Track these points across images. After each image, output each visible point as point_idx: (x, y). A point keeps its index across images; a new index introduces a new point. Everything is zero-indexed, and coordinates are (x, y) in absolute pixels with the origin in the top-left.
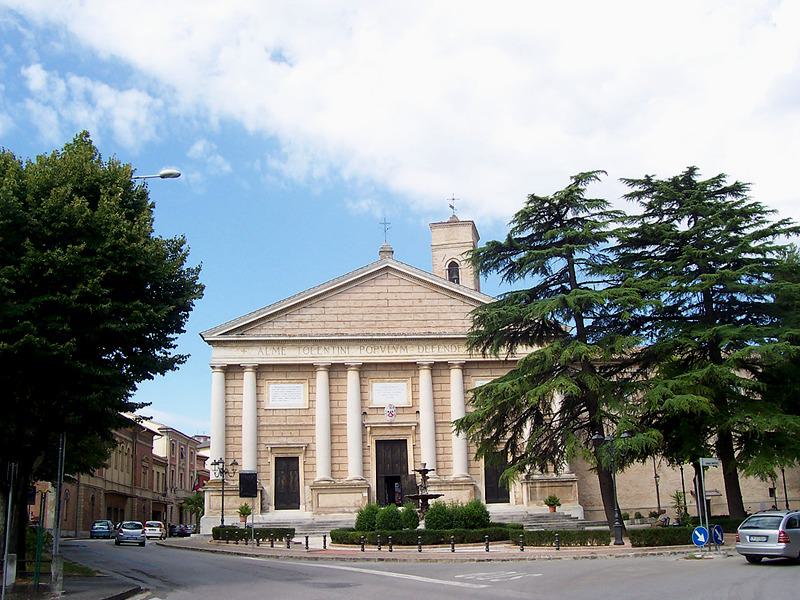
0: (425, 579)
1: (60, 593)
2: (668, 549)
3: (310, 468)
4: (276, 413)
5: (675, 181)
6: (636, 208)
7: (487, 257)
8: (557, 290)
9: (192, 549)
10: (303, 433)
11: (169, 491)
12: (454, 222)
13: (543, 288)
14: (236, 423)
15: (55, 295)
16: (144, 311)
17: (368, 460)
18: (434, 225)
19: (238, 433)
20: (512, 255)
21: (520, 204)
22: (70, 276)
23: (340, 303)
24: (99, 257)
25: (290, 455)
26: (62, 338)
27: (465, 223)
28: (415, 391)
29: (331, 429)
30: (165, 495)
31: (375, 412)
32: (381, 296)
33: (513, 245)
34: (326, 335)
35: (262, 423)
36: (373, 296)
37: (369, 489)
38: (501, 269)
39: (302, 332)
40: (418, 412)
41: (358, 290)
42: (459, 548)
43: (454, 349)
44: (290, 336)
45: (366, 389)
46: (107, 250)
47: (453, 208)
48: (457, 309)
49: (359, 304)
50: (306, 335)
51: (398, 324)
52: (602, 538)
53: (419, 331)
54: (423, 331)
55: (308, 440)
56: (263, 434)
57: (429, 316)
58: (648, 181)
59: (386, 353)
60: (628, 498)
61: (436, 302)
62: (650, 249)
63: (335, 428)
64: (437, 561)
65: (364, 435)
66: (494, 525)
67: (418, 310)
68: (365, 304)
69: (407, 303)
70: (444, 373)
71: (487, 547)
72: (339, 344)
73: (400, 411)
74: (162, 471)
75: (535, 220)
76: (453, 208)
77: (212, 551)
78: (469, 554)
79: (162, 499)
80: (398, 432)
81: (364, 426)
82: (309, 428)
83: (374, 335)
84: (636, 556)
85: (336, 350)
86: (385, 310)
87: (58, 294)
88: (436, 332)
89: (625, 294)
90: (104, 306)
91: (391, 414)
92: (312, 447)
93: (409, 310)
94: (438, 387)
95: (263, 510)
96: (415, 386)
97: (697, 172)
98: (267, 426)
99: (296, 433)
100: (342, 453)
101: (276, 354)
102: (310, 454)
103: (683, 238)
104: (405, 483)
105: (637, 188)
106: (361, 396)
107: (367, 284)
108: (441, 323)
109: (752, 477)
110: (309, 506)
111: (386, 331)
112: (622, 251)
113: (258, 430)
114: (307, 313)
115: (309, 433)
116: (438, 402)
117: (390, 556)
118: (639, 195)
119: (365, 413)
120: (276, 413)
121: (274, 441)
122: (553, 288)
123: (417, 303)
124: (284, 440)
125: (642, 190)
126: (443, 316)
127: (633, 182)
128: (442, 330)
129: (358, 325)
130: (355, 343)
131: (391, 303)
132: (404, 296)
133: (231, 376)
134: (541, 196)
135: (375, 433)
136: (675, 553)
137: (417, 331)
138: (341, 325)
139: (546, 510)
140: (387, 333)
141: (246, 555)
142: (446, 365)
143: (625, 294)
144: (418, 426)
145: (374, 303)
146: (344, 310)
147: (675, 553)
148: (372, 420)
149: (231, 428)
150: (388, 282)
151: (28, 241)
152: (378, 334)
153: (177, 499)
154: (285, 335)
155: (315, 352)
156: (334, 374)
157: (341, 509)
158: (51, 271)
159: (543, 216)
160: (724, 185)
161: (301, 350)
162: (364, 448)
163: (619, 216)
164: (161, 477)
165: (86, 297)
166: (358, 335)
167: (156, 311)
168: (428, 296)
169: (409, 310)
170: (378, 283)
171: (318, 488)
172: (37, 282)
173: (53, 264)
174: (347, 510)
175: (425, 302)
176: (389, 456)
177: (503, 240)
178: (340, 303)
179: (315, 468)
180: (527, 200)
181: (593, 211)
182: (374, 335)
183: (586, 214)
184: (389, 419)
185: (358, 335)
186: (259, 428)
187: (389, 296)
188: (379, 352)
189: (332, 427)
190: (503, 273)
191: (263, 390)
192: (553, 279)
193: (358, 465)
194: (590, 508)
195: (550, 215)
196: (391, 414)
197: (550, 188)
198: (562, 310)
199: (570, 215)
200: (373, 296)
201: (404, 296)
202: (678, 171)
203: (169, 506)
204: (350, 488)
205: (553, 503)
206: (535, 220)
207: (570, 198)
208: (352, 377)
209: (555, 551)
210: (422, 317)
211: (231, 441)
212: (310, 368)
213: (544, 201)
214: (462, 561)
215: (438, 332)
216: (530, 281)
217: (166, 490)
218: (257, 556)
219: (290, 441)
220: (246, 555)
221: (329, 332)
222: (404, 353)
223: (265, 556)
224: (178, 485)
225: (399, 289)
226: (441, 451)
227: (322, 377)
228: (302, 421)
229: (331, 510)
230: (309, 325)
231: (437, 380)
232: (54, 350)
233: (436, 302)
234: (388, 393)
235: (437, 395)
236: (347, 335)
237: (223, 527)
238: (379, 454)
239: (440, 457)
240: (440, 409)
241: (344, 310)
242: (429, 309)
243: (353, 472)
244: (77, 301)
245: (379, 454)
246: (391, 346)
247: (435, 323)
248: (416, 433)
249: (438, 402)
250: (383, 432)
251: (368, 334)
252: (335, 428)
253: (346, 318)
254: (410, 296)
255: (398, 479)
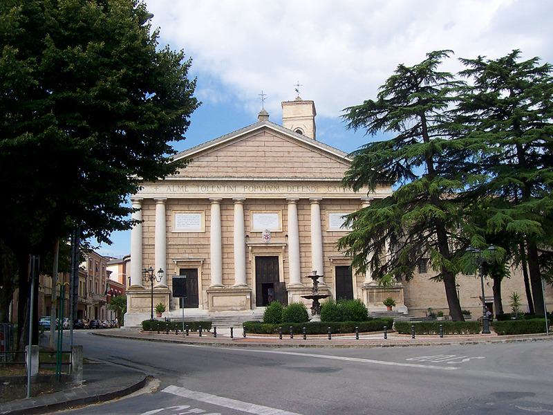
0: (374, 361)
1: (81, 382)
2: (531, 337)
3: (207, 277)
4: (181, 235)
5: (501, 61)
6: (471, 81)
7: (361, 113)
8: (409, 142)
9: (130, 338)
10: (200, 251)
11: (88, 295)
12: (298, 102)
13: (399, 140)
14: (150, 243)
15: (75, 91)
16: (155, 113)
17: (249, 271)
18: (284, 104)
19: (151, 251)
20: (378, 113)
21: (392, 72)
22: (88, 76)
23: (229, 154)
24: (116, 59)
25: (191, 267)
26: (83, 133)
27: (307, 102)
28: (284, 221)
29: (222, 248)
30: (85, 298)
31: (254, 235)
32: (260, 149)
33: (381, 105)
34: (219, 177)
35: (169, 243)
36: (254, 149)
37: (251, 293)
38: (368, 123)
39: (200, 174)
40: (287, 236)
41: (233, 149)
42: (362, 337)
43: (314, 189)
44: (191, 177)
45: (248, 218)
46: (122, 53)
47: (297, 91)
48: (316, 160)
49: (243, 154)
50: (203, 177)
51: (273, 170)
52: (444, 329)
53: (288, 176)
54: (291, 175)
55: (205, 256)
56: (170, 251)
58: (478, 62)
59: (273, 191)
60: (436, 301)
61: (300, 154)
62: (480, 112)
63: (225, 247)
64: (349, 346)
65: (246, 253)
66: (371, 319)
67: (287, 159)
68: (248, 154)
69: (279, 154)
70: (305, 207)
71: (385, 335)
72: (228, 183)
73: (274, 235)
74: (83, 280)
75: (398, 86)
76: (297, 91)
77: (150, 340)
78: (373, 340)
79: (84, 301)
80: (272, 250)
81: (246, 246)
82: (205, 246)
83: (255, 177)
84: (507, 342)
85: (226, 189)
86: (262, 159)
87: (78, 89)
88: (300, 176)
89: (475, 142)
90: (122, 104)
91: (267, 237)
92: (208, 261)
93: (281, 160)
94: (301, 218)
95: (171, 308)
96: (284, 216)
97: (519, 55)
98: (174, 245)
99: (196, 251)
100: (231, 266)
101: (181, 191)
102: (206, 266)
103: (506, 102)
104: (277, 289)
105: (470, 67)
106: (245, 224)
107: (249, 139)
108: (305, 170)
110: (205, 305)
111: (263, 175)
112: (458, 113)
113: (167, 248)
114: (204, 161)
115: (205, 251)
116: (302, 228)
117: (304, 342)
118: (469, 72)
119: (247, 236)
120: (181, 235)
121: (179, 257)
122: (406, 140)
123: (286, 154)
124: (187, 256)
125: (472, 68)
127: (467, 62)
128: (305, 175)
129: (242, 170)
130: (239, 183)
131: (267, 154)
132: (277, 149)
134: (407, 67)
135: (255, 251)
136: (535, 340)
137: (286, 175)
138: (230, 170)
139: (384, 309)
140: (264, 176)
141: (182, 343)
143: (475, 142)
144: (287, 246)
145: (255, 154)
146: (232, 159)
147: (535, 340)
148: (252, 241)
149: (146, 247)
150: (266, 138)
151: (48, 36)
152: (258, 177)
153: (94, 301)
154: (187, 177)
155: (210, 190)
156: (224, 207)
157: (230, 308)
158: (71, 67)
159: (404, 84)
160: (536, 66)
161: (200, 188)
162: (247, 263)
163: (461, 85)
164: (82, 284)
165: (104, 94)
166: (243, 177)
167: (167, 113)
168: (295, 149)
169: (281, 160)
170: (258, 139)
171: (212, 292)
172: (56, 75)
173: (74, 59)
174: (234, 308)
176: (265, 269)
177: (375, 100)
178: (229, 154)
179: (211, 277)
180: (396, 69)
181: (439, 82)
182: (255, 177)
183: (434, 84)
184: (265, 241)
185: (243, 177)
186: (167, 246)
187: (266, 149)
188: (258, 191)
189: (223, 246)
190: (368, 128)
191: (170, 218)
192: (407, 133)
193: (241, 274)
194: (411, 308)
195: (409, 82)
196: (267, 237)
197: (413, 59)
199: (423, 85)
200: (254, 149)
201: (277, 149)
202: (503, 53)
203: (88, 307)
204: (237, 292)
205: (390, 303)
206: (398, 86)
207: (424, 70)
208: (238, 209)
209: (440, 338)
210: (290, 165)
211: (146, 256)
212: (206, 202)
213: (407, 70)
214: (370, 347)
215: (302, 177)
216: (386, 135)
217: (86, 294)
218: (192, 343)
219: (191, 256)
220: (182, 343)
221: (221, 174)
222: (277, 192)
223: (199, 344)
224: (94, 291)
225: (273, 144)
226: (303, 265)
227: (215, 208)
228: (201, 242)
229: (223, 308)
230: (206, 169)
231: (300, 212)
232: (76, 145)
233: (300, 154)
234: (264, 222)
235: (301, 223)
236: (234, 177)
237: (152, 320)
238: (258, 267)
239: (303, 270)
240: (303, 234)
241: (232, 159)
242: (295, 159)
243: (238, 280)
244: (96, 98)
245: (258, 267)
246: (280, 187)
247: (300, 170)
248: (285, 251)
249: (302, 228)
250: (261, 251)
251: (250, 177)
252: (225, 247)
253: (233, 164)
254: (281, 149)
255: (271, 286)
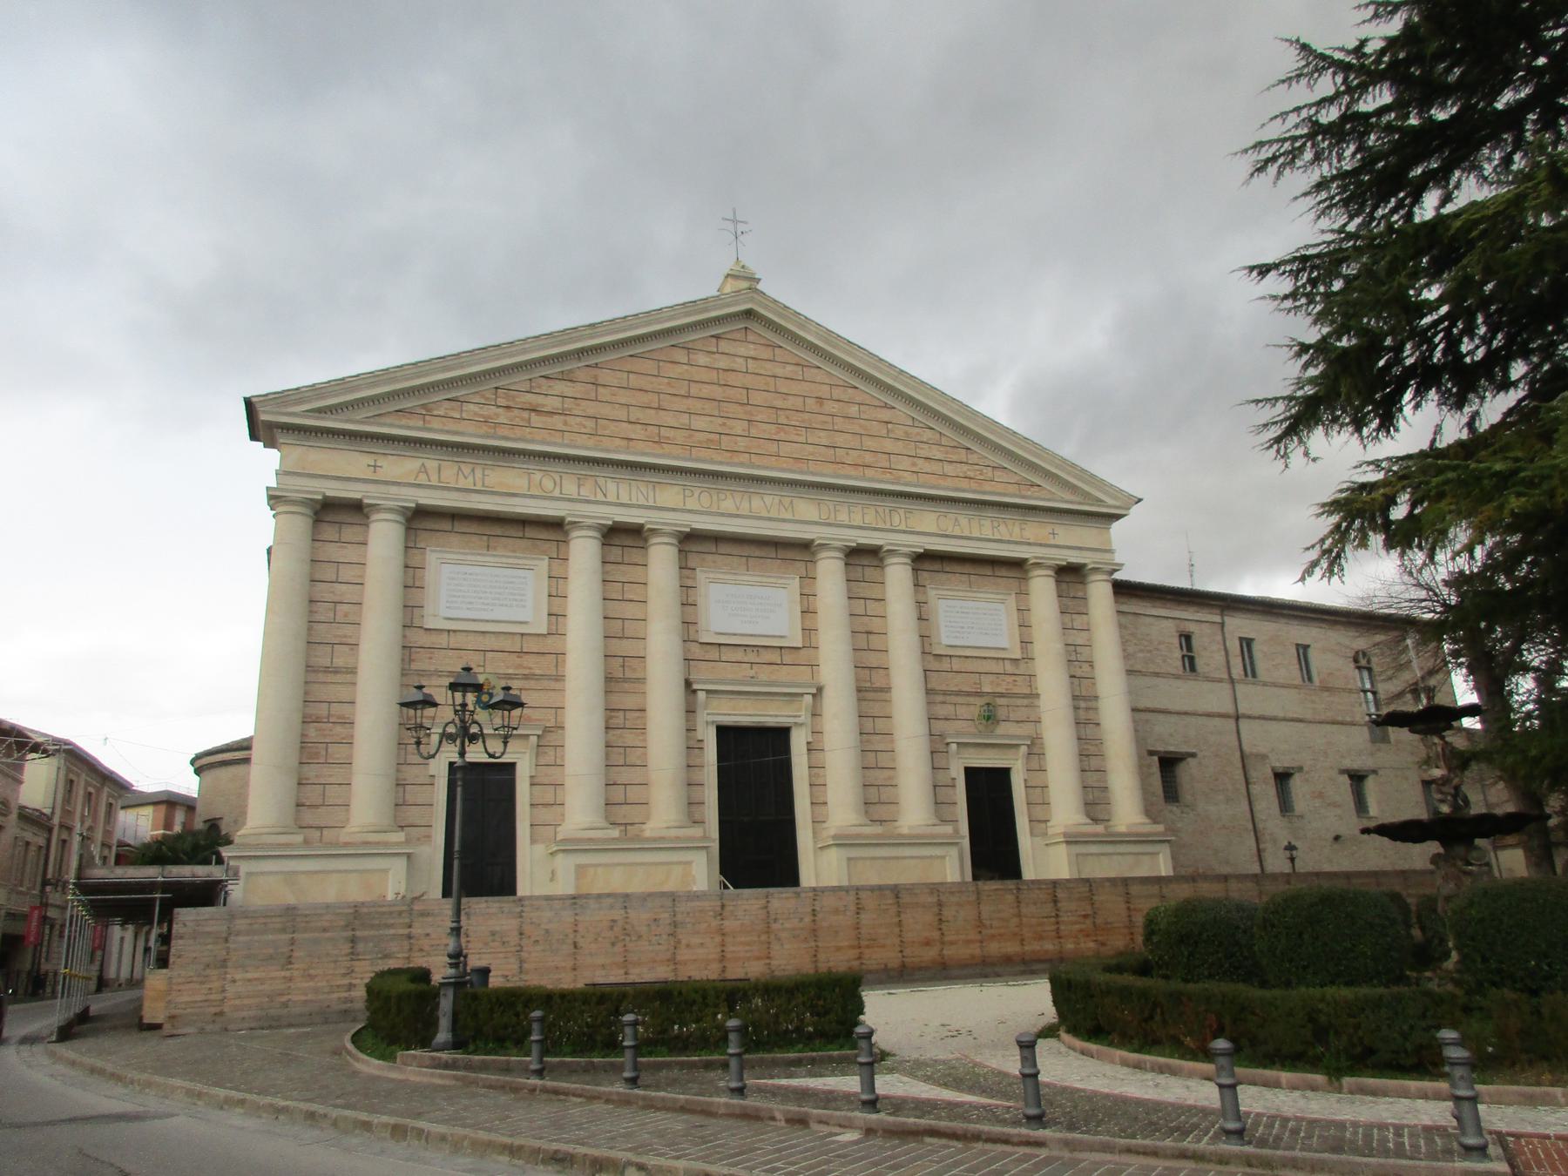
28: (557, 595)
31: (713, 654)
32: (732, 379)
35: (414, 666)
57: (840, 439)
65: (690, 711)
69: (791, 402)
82: (546, 684)
96: (557, 580)
109: (825, 970)
126: (870, 443)
131: (757, 398)
133: (329, 532)
142: (357, 509)
145: (718, 392)
169: (796, 419)
175: (830, 407)
198: (1511, 529)
249: (323, 613)
